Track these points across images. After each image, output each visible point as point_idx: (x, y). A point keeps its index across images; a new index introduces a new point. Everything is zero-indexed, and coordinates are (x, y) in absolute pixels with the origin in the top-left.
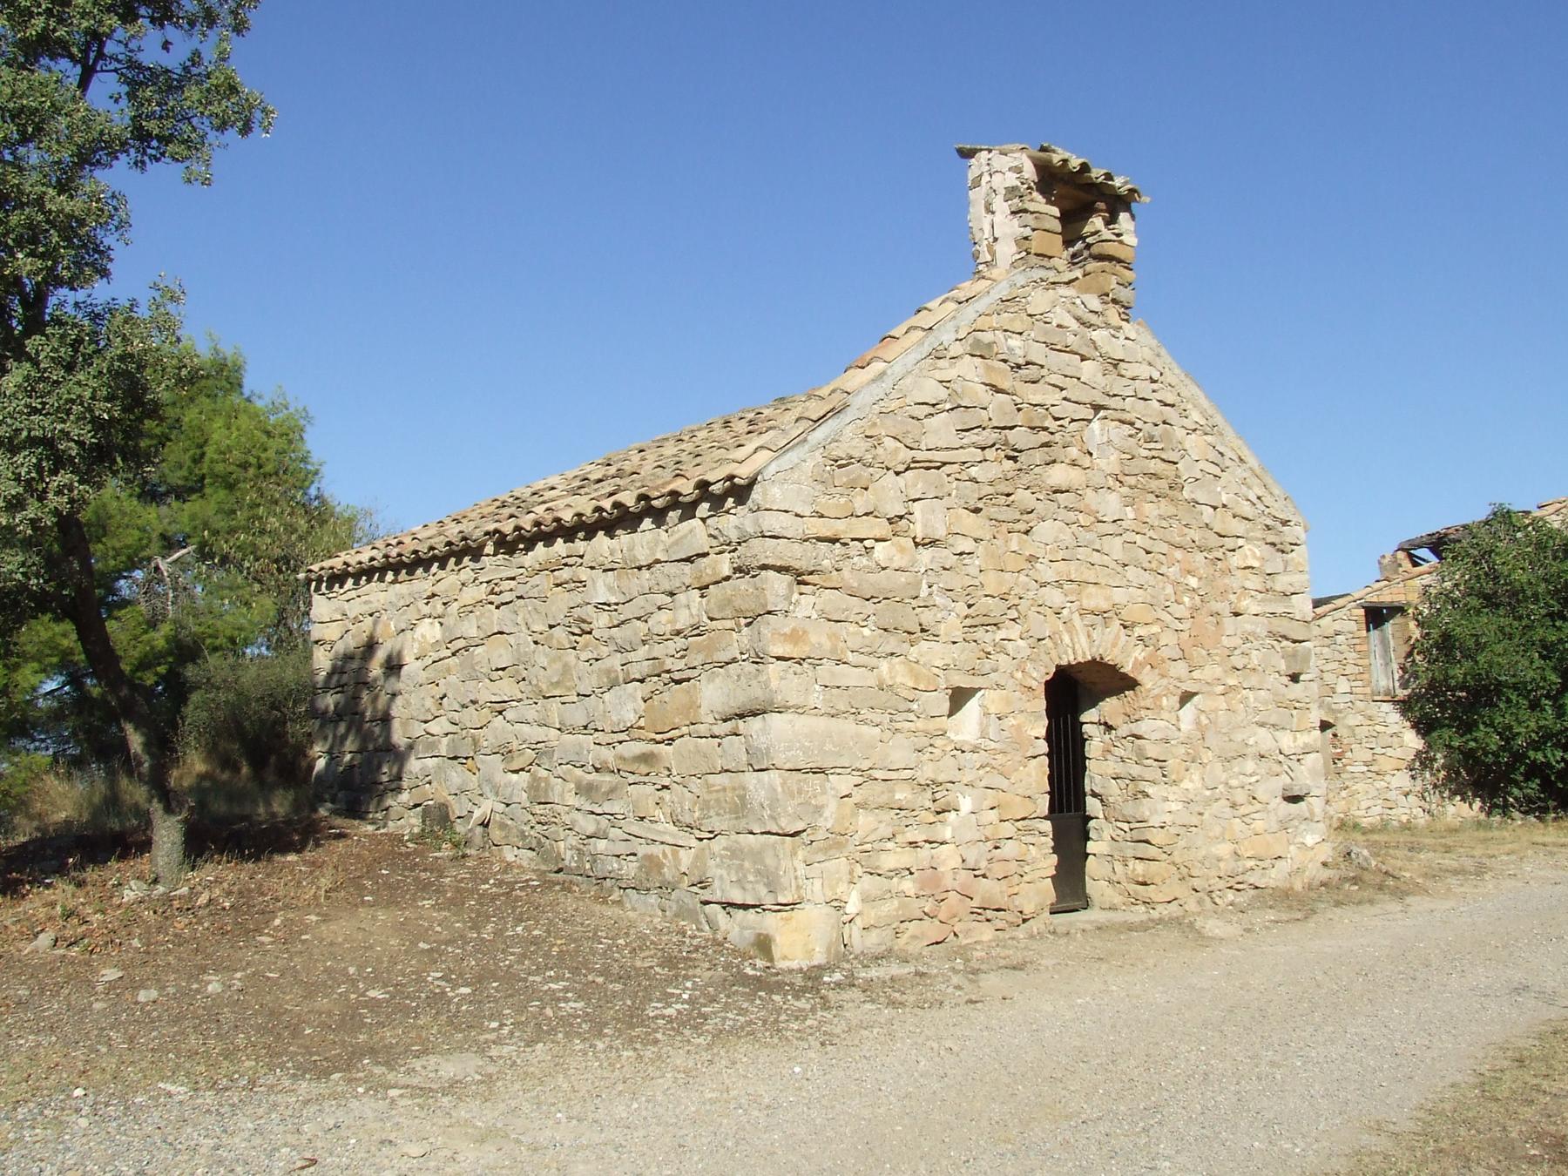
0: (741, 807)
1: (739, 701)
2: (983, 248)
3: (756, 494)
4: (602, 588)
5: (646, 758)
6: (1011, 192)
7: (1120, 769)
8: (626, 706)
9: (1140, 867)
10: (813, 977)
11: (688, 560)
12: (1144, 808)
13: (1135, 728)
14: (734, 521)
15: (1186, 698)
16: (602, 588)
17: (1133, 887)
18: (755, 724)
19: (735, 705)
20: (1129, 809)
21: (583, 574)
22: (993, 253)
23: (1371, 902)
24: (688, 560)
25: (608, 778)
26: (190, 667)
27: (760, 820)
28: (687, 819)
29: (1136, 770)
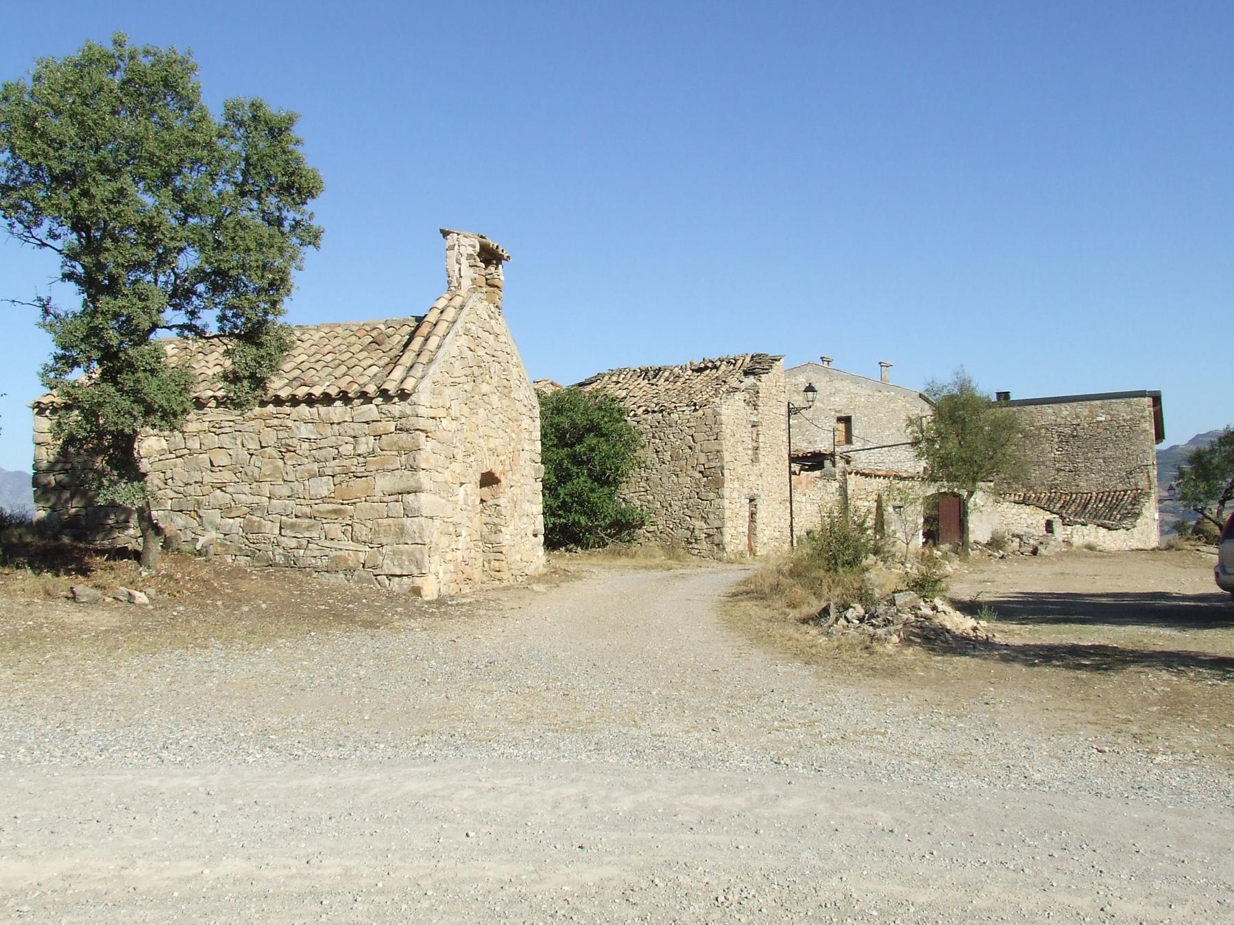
0: (402, 531)
1: (402, 486)
2: (454, 280)
3: (413, 398)
4: (305, 431)
5: (335, 512)
6: (470, 256)
7: (488, 520)
8: (323, 487)
9: (497, 564)
10: (440, 602)
11: (367, 423)
12: (501, 537)
13: (496, 501)
14: (397, 408)
15: (462, 484)
16: (305, 431)
17: (493, 573)
18: (411, 497)
19: (398, 488)
20: (493, 538)
21: (290, 423)
22: (460, 284)
23: (1083, 524)
24: (367, 423)
25: (307, 520)
26: (1215, 559)
27: (414, 538)
28: (364, 539)
29: (497, 521)
